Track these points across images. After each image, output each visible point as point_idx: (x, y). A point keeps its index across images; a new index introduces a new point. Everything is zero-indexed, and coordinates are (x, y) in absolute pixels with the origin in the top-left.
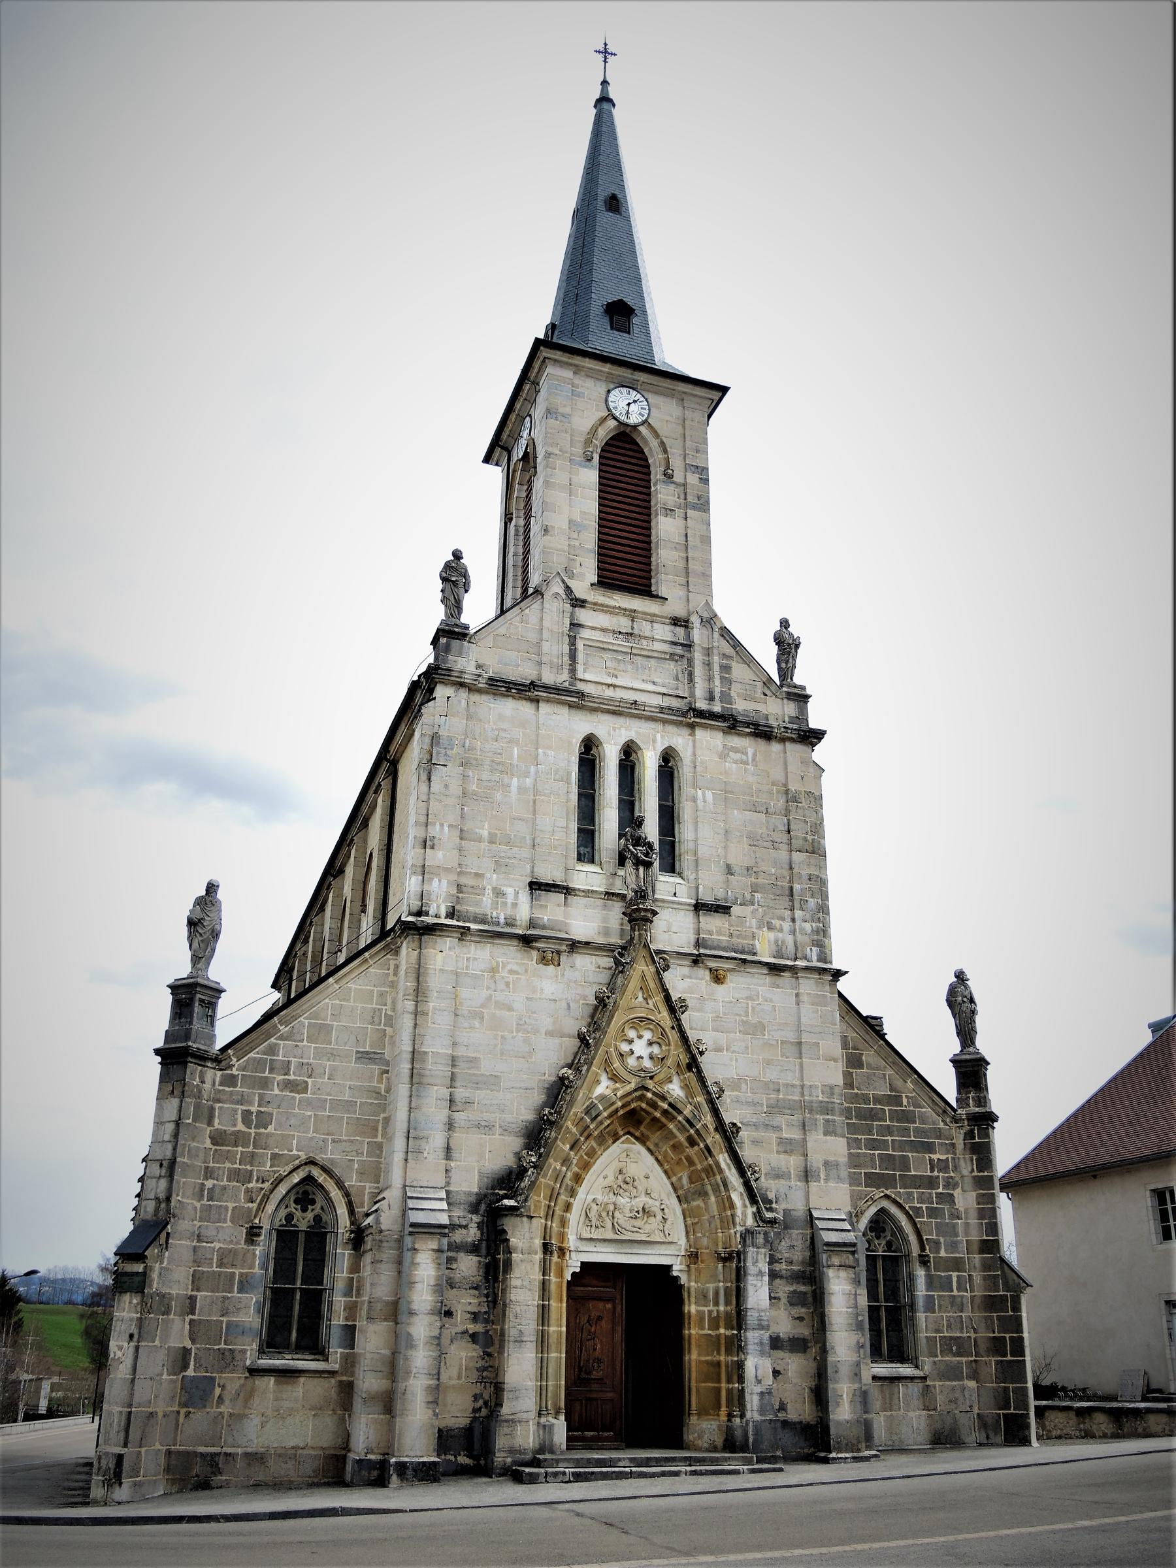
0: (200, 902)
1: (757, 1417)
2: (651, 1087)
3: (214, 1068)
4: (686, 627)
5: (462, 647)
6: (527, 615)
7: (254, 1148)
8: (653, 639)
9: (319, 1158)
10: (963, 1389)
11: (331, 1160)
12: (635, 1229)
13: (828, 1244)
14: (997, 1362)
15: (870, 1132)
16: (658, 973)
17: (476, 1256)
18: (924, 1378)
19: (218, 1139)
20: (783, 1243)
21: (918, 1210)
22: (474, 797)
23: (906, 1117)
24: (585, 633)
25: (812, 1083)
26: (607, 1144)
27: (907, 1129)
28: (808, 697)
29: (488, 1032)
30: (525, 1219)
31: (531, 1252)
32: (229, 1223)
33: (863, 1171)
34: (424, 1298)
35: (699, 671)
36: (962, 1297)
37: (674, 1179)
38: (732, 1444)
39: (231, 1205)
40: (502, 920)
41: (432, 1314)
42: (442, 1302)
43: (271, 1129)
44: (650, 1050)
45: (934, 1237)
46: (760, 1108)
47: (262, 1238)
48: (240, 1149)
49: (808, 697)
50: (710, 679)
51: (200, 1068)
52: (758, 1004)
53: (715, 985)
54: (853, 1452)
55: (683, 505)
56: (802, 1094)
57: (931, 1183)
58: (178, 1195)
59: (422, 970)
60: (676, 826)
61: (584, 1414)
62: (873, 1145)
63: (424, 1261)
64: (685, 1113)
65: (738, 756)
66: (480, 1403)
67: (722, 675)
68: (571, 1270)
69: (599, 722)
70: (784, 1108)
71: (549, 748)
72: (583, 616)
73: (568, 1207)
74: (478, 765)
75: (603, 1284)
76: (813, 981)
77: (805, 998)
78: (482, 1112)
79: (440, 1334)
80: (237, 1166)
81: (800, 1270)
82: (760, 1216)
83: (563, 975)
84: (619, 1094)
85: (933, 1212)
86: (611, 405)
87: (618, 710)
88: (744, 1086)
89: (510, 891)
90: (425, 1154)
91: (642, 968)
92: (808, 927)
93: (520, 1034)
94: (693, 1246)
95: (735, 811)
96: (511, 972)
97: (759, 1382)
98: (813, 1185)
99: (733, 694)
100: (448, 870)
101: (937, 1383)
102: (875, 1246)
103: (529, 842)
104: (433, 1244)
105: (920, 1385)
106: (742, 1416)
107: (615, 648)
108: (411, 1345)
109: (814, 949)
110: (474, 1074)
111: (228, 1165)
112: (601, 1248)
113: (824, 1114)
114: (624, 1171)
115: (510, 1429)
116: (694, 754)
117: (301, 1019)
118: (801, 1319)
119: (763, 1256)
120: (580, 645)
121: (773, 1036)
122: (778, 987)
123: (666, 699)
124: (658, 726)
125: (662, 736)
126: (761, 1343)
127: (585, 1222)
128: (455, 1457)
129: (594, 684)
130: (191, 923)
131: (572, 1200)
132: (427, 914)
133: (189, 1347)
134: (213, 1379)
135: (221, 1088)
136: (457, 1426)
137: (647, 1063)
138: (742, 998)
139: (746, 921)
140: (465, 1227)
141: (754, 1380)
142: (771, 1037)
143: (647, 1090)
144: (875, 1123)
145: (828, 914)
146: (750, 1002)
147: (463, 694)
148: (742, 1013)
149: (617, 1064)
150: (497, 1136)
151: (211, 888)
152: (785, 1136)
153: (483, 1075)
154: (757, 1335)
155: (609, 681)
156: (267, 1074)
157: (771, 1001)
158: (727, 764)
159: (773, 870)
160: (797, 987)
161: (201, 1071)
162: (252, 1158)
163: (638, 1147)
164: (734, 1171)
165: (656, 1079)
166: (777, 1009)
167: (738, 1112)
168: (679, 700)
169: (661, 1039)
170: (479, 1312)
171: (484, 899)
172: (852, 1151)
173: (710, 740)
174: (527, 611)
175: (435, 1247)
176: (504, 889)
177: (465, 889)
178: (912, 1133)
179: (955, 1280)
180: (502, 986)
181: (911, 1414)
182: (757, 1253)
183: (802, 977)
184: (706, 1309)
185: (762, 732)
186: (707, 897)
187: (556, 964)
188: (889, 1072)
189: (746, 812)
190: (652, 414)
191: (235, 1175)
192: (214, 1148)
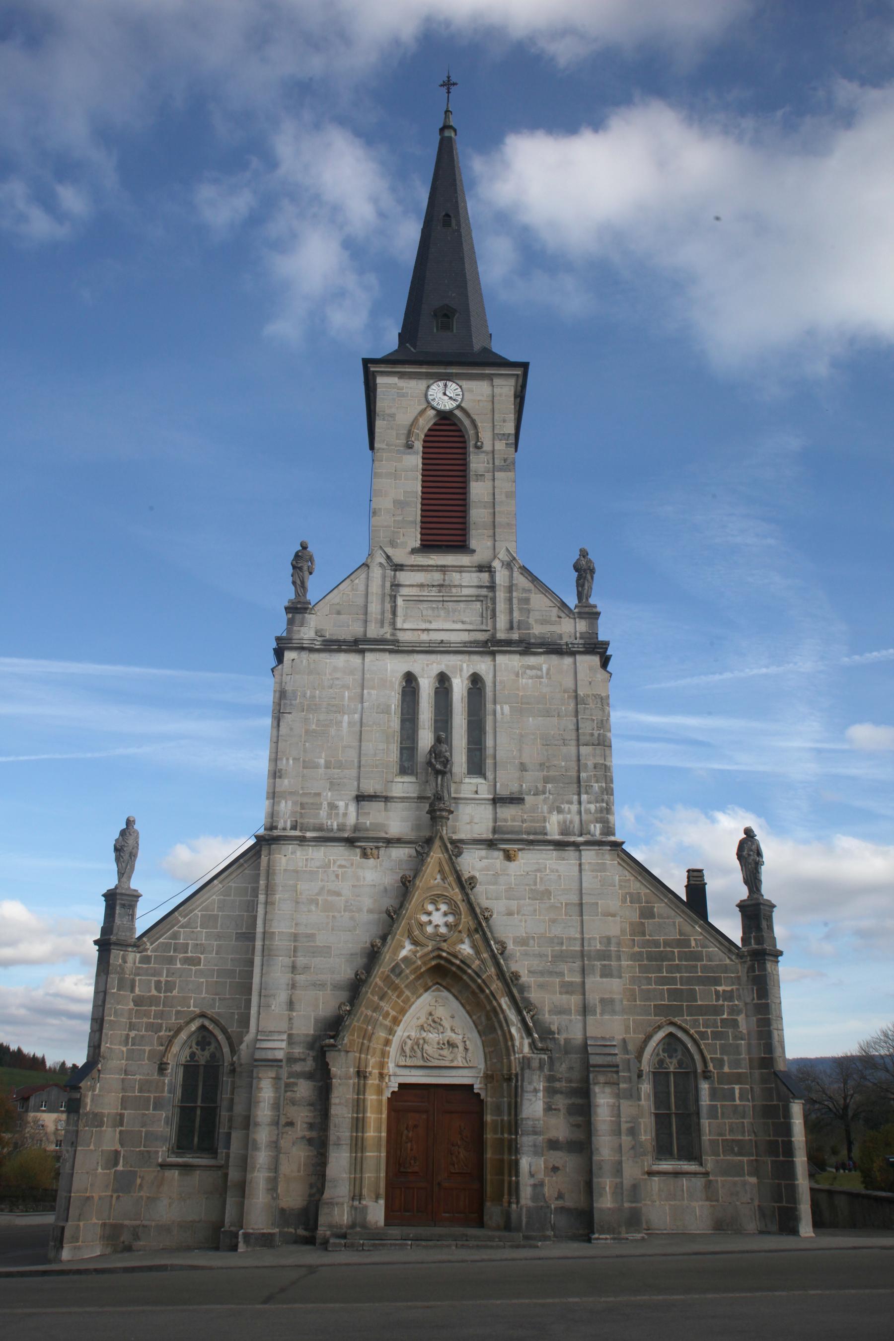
0: (123, 833)
1: (530, 1203)
2: (445, 948)
3: (134, 952)
4: (490, 571)
5: (303, 618)
6: (357, 584)
7: (164, 1006)
8: (461, 586)
9: (209, 1012)
10: (744, 1184)
11: (219, 1014)
12: (441, 1058)
14: (772, 1162)
15: (660, 970)
16: (451, 859)
18: (707, 1174)
19: (138, 1002)
20: (564, 1066)
21: (703, 1035)
23: (697, 956)
24: (404, 591)
26: (419, 993)
27: (696, 966)
28: (598, 614)
29: (322, 914)
30: (343, 1053)
32: (147, 1062)
33: (652, 1003)
34: (265, 1113)
35: (501, 606)
36: (744, 1106)
37: (474, 1017)
38: (507, 1226)
39: (147, 1048)
40: (335, 827)
43: (175, 992)
44: (445, 919)
45: (718, 1056)
47: (169, 1071)
48: (153, 1008)
49: (598, 614)
50: (511, 611)
51: (122, 953)
53: (507, 863)
54: (614, 1234)
55: (491, 469)
57: (717, 1010)
58: (106, 1043)
59: (271, 871)
60: (483, 736)
62: (663, 981)
65: (534, 672)
66: (314, 1190)
67: (521, 606)
68: (392, 1090)
69: (415, 661)
71: (373, 688)
72: (404, 577)
73: (387, 1043)
76: (593, 852)
78: (317, 975)
80: (152, 1020)
84: (418, 955)
85: (716, 1035)
86: (430, 398)
87: (430, 650)
88: (531, 942)
89: (341, 804)
90: (273, 1007)
91: (436, 855)
92: (592, 807)
93: (347, 913)
96: (341, 866)
99: (531, 621)
101: (719, 1179)
102: (667, 1064)
103: (356, 764)
105: (703, 1180)
106: (518, 1202)
107: (429, 599)
108: (256, 1148)
109: (598, 825)
111: (145, 1020)
112: (414, 1072)
114: (433, 1013)
116: (495, 676)
117: (196, 912)
120: (400, 601)
122: (563, 859)
123: (472, 633)
124: (465, 657)
125: (468, 665)
126: (535, 1146)
127: (401, 1054)
128: (296, 1230)
129: (411, 632)
130: (117, 849)
131: (391, 1037)
132: (276, 828)
133: (119, 1149)
134: (135, 1173)
135: (140, 965)
137: (443, 930)
138: (531, 871)
139: (538, 808)
140: (304, 1060)
142: (556, 901)
144: (665, 963)
145: (612, 794)
146: (538, 874)
147: (305, 655)
149: (416, 932)
151: (129, 823)
152: (567, 979)
153: (317, 946)
155: (424, 626)
156: (172, 953)
157: (557, 871)
158: (524, 680)
159: (563, 764)
161: (123, 955)
162: (161, 1015)
163: (446, 994)
164: (513, 1011)
165: (449, 941)
167: (526, 963)
168: (483, 633)
169: (454, 910)
171: (321, 812)
172: (643, 987)
173: (508, 662)
174: (357, 581)
175: (274, 1075)
178: (699, 970)
179: (737, 1092)
180: (333, 878)
181: (694, 1204)
183: (583, 850)
185: (554, 648)
186: (502, 791)
187: (376, 857)
188: (679, 920)
189: (540, 718)
190: (465, 397)
191: (150, 1027)
192: (135, 1008)
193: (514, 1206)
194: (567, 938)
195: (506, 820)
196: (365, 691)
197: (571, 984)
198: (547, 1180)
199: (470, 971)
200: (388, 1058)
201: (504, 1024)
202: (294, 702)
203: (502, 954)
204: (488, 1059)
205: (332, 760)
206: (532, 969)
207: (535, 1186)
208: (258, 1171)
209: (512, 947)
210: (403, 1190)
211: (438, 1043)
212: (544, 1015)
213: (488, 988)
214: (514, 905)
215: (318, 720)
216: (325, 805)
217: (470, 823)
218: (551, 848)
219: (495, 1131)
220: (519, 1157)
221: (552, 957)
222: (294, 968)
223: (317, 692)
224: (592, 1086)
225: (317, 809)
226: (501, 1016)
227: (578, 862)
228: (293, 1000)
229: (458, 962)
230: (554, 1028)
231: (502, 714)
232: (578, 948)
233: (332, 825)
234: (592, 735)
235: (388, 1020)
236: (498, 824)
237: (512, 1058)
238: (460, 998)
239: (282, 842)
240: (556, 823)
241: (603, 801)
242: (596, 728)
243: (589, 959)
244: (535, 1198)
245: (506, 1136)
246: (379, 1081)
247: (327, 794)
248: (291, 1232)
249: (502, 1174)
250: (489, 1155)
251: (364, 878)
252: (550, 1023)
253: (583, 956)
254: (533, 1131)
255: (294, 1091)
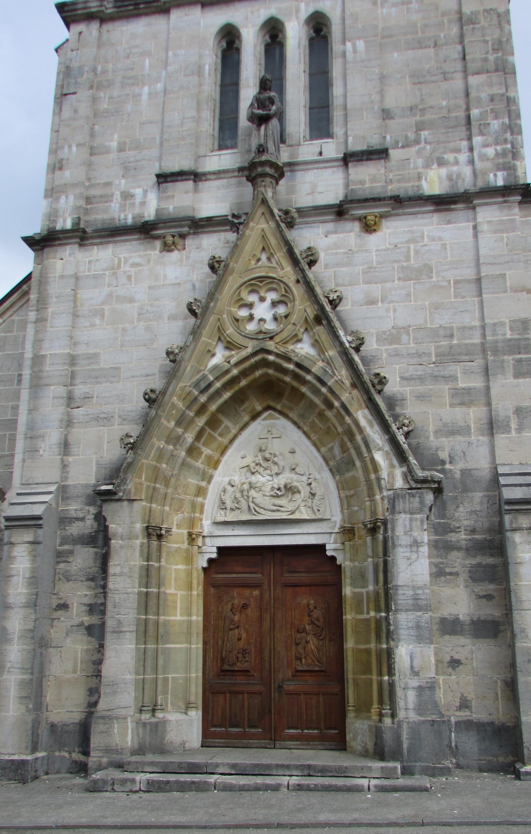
1: (413, 716)
13: (510, 502)
17: (93, 547)
20: (461, 509)
22: (105, 115)
25: (496, 321)
31: (131, 537)
34: (19, 591)
41: (27, 607)
42: (37, 595)
46: (426, 359)
52: (422, 246)
56: (484, 336)
61: (228, 708)
63: (20, 554)
64: (313, 370)
68: (207, 556)
70: (460, 354)
73: (201, 492)
74: (110, 84)
75: (248, 570)
77: (485, 227)
79: (34, 627)
81: (485, 540)
82: (412, 476)
83: (188, 258)
84: (233, 361)
88: (404, 338)
89: (138, 192)
90: (41, 452)
93: (141, 323)
94: (347, 521)
95: (395, 55)
96: (134, 265)
97: (415, 673)
98: (501, 439)
100: (75, 185)
104: (28, 536)
106: (393, 716)
109: (499, 174)
110: (94, 370)
113: (515, 353)
115: (107, 726)
116: (343, 11)
118: (489, 597)
119: (418, 523)
121: (443, 277)
122: (449, 222)
126: (418, 627)
127: (219, 506)
136: (72, 721)
137: (270, 326)
138: (402, 243)
139: (409, 163)
140: (82, 519)
141: (408, 672)
142: (440, 279)
143: (269, 352)
145: (520, 133)
146: (412, 246)
147: (95, 26)
148: (402, 258)
149: (230, 330)
150: (116, 427)
152: (461, 385)
153: (102, 369)
154: (411, 617)
157: (440, 239)
158: (385, 10)
160: (475, 219)
163: (282, 422)
164: (376, 427)
166: (448, 247)
167: (398, 367)
170: (96, 604)
171: (112, 205)
175: (31, 539)
176: (132, 191)
177: (94, 200)
180: (123, 280)
182: (411, 520)
184: (364, 590)
189: (409, 52)
193: (388, 721)
194: (459, 329)
195: (362, 182)
196: (170, 53)
197: (468, 391)
198: (441, 679)
199: (309, 378)
200: (202, 512)
201: (364, 449)
202: (79, 80)
203: (357, 349)
204: (345, 507)
205: (127, 140)
206: (406, 375)
207: (420, 689)
208: (9, 671)
209: (375, 346)
210: (228, 695)
211: (273, 488)
212: (428, 438)
213: (338, 398)
214: (376, 290)
215: (111, 98)
216: (117, 195)
217: (312, 193)
218: (431, 208)
219: (359, 610)
220: (392, 643)
221: (436, 356)
222: (70, 398)
223: (111, 65)
224: (508, 534)
225: (106, 202)
226: (359, 438)
227: (471, 224)
228: (69, 441)
229: (291, 367)
230: (444, 455)
231: (355, 51)
232: (477, 340)
233: (126, 219)
234: (486, 60)
235: (200, 461)
236: (351, 187)
237: (378, 497)
238: (301, 424)
239: (57, 243)
240: (436, 179)
241: (506, 141)
242: (491, 51)
243: (495, 352)
244: (420, 709)
245: (372, 614)
246: (189, 544)
247: (120, 183)
248: (64, 757)
249: (369, 672)
250: (350, 644)
251: (165, 276)
252: (437, 449)
253: (484, 351)
254: (413, 605)
255: (70, 562)
